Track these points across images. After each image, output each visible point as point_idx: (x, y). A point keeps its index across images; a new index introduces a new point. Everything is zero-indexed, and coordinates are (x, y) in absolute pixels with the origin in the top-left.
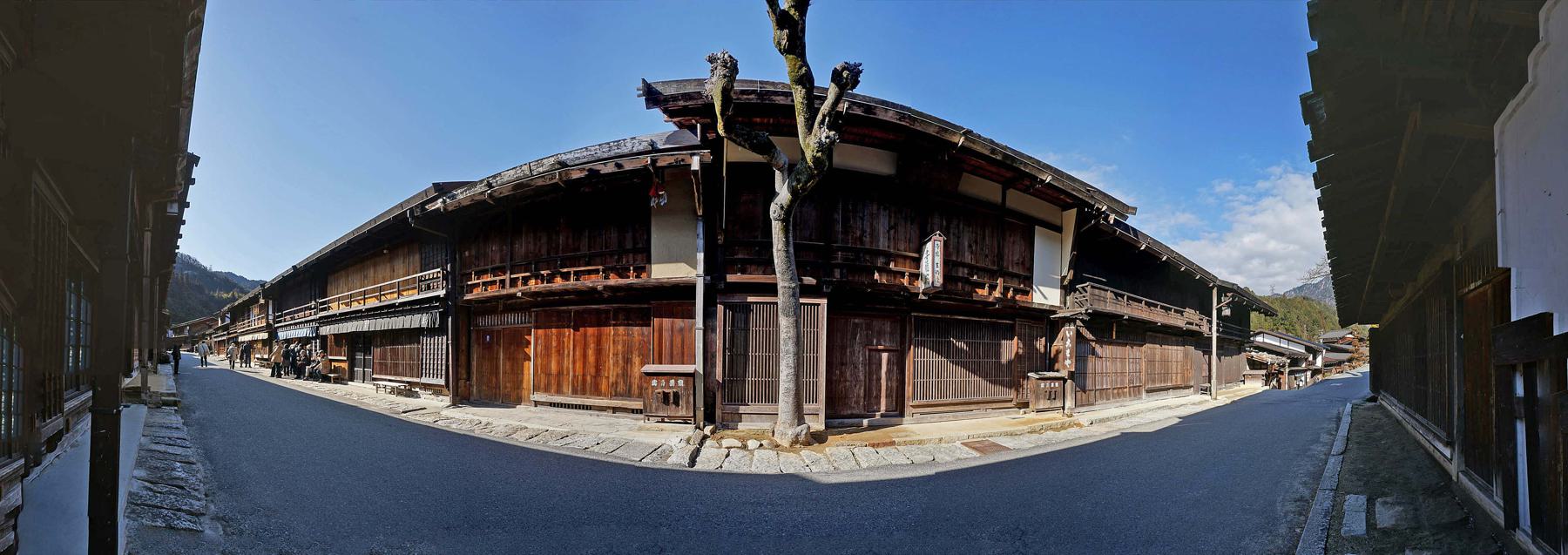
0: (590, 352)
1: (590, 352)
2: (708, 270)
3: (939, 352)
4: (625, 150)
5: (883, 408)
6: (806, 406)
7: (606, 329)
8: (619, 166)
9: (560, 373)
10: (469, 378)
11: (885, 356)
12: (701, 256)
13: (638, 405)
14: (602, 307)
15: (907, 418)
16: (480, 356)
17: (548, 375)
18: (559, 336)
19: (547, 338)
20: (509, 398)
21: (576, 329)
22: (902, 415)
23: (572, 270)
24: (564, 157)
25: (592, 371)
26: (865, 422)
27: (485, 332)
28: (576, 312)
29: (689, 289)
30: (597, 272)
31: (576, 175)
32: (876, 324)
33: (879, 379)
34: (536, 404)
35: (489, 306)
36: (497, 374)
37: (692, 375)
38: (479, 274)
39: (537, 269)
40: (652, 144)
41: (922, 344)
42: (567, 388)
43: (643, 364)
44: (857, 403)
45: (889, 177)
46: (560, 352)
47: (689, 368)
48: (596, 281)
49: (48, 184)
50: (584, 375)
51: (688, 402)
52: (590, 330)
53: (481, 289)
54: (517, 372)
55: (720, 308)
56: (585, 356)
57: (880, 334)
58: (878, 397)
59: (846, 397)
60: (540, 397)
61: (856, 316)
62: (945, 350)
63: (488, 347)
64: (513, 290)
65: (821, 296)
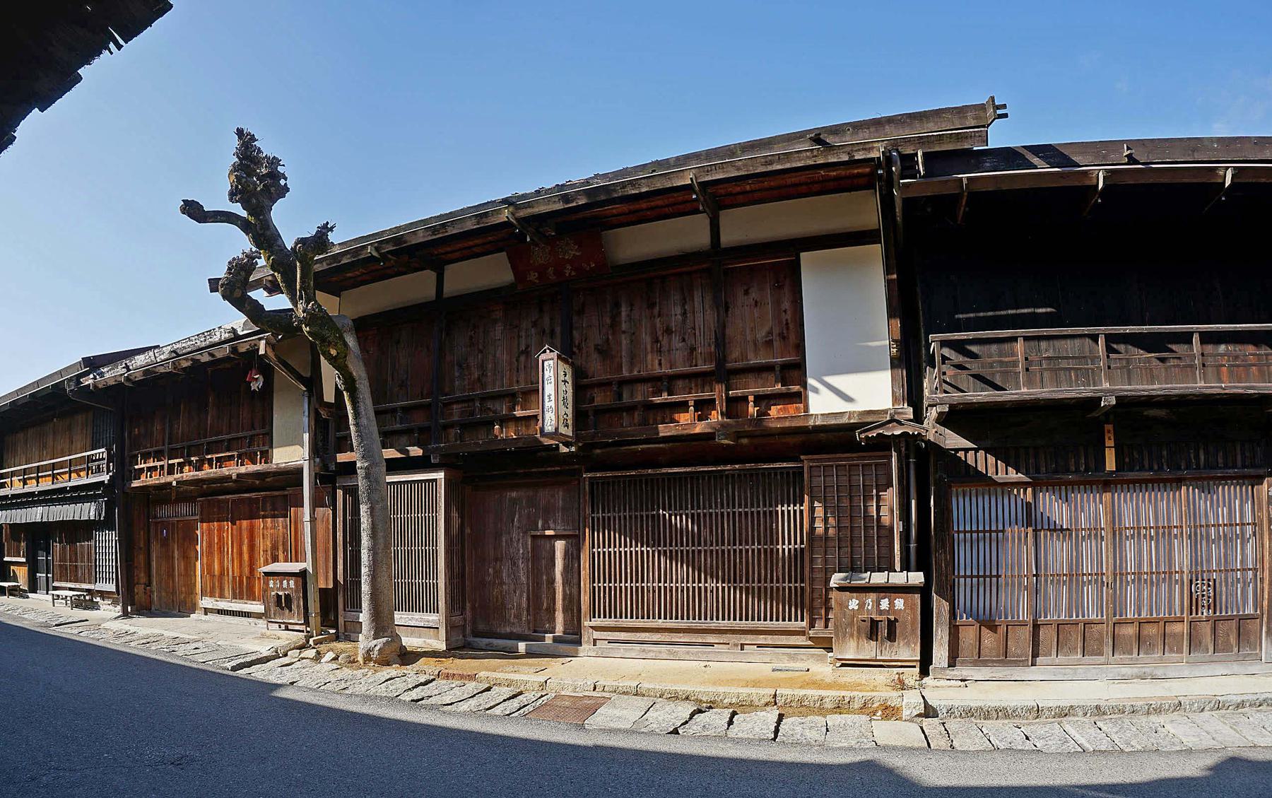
0: (245, 548)
1: (245, 548)
2: (316, 451)
3: (639, 539)
4: (216, 339)
5: (559, 629)
6: (400, 617)
7: (259, 523)
8: (211, 355)
9: (222, 574)
10: (149, 584)
11: (560, 545)
12: (306, 436)
13: (258, 607)
14: (253, 495)
15: (585, 648)
16: (150, 553)
17: (213, 576)
18: (220, 530)
19: (220, 530)
20: (183, 607)
21: (234, 523)
22: (579, 642)
23: (214, 456)
24: (175, 347)
25: (246, 570)
26: (522, 647)
27: (165, 525)
28: (234, 501)
29: (298, 472)
30: (231, 458)
31: (185, 364)
32: (543, 495)
33: (552, 581)
34: (206, 611)
35: (161, 494)
36: (173, 576)
37: (303, 574)
38: (146, 457)
39: (189, 455)
40: (234, 331)
41: (605, 525)
42: (228, 591)
43: (267, 563)
44: (518, 616)
45: (511, 286)
46: (221, 551)
47: (295, 567)
48: (233, 470)
49: (71, 589)
50: (241, 577)
51: (298, 606)
52: (245, 523)
53: (151, 474)
54: (189, 572)
55: (340, 493)
56: (241, 554)
57: (548, 513)
58: (551, 610)
59: (503, 606)
60: (207, 602)
61: (514, 487)
62: (654, 534)
63: (165, 543)
64: (169, 479)
65: (434, 468)
